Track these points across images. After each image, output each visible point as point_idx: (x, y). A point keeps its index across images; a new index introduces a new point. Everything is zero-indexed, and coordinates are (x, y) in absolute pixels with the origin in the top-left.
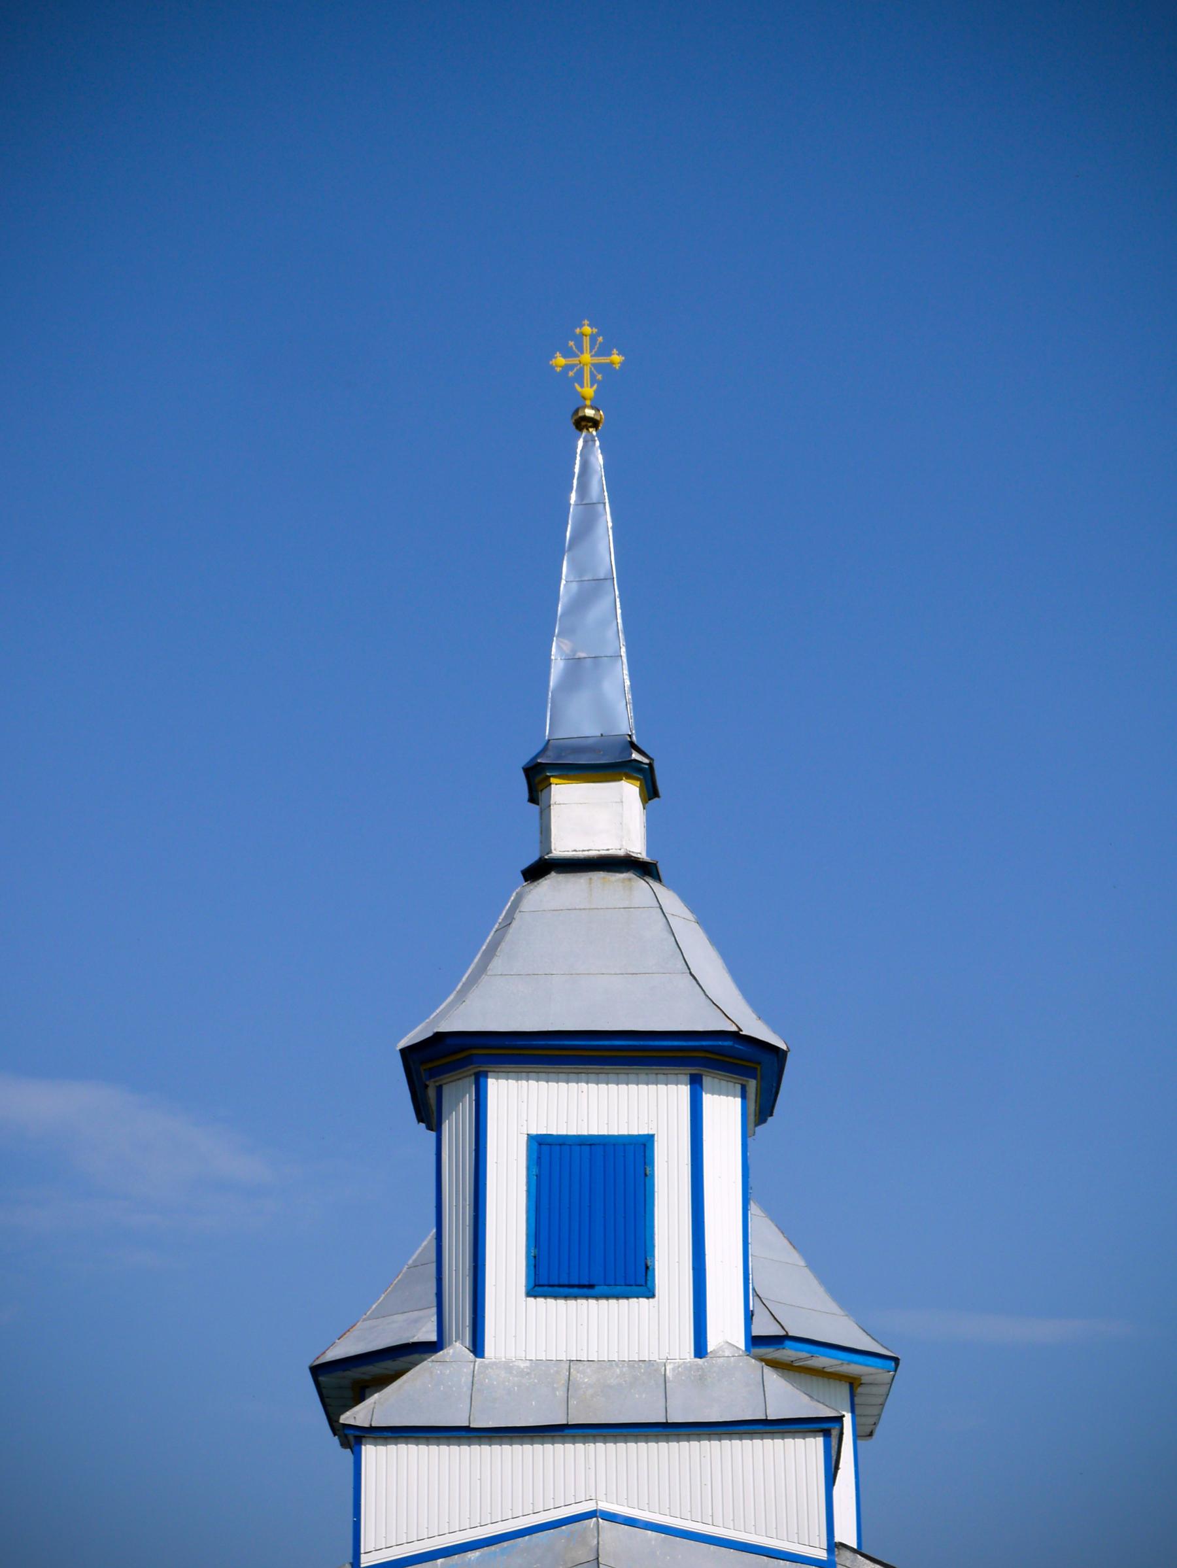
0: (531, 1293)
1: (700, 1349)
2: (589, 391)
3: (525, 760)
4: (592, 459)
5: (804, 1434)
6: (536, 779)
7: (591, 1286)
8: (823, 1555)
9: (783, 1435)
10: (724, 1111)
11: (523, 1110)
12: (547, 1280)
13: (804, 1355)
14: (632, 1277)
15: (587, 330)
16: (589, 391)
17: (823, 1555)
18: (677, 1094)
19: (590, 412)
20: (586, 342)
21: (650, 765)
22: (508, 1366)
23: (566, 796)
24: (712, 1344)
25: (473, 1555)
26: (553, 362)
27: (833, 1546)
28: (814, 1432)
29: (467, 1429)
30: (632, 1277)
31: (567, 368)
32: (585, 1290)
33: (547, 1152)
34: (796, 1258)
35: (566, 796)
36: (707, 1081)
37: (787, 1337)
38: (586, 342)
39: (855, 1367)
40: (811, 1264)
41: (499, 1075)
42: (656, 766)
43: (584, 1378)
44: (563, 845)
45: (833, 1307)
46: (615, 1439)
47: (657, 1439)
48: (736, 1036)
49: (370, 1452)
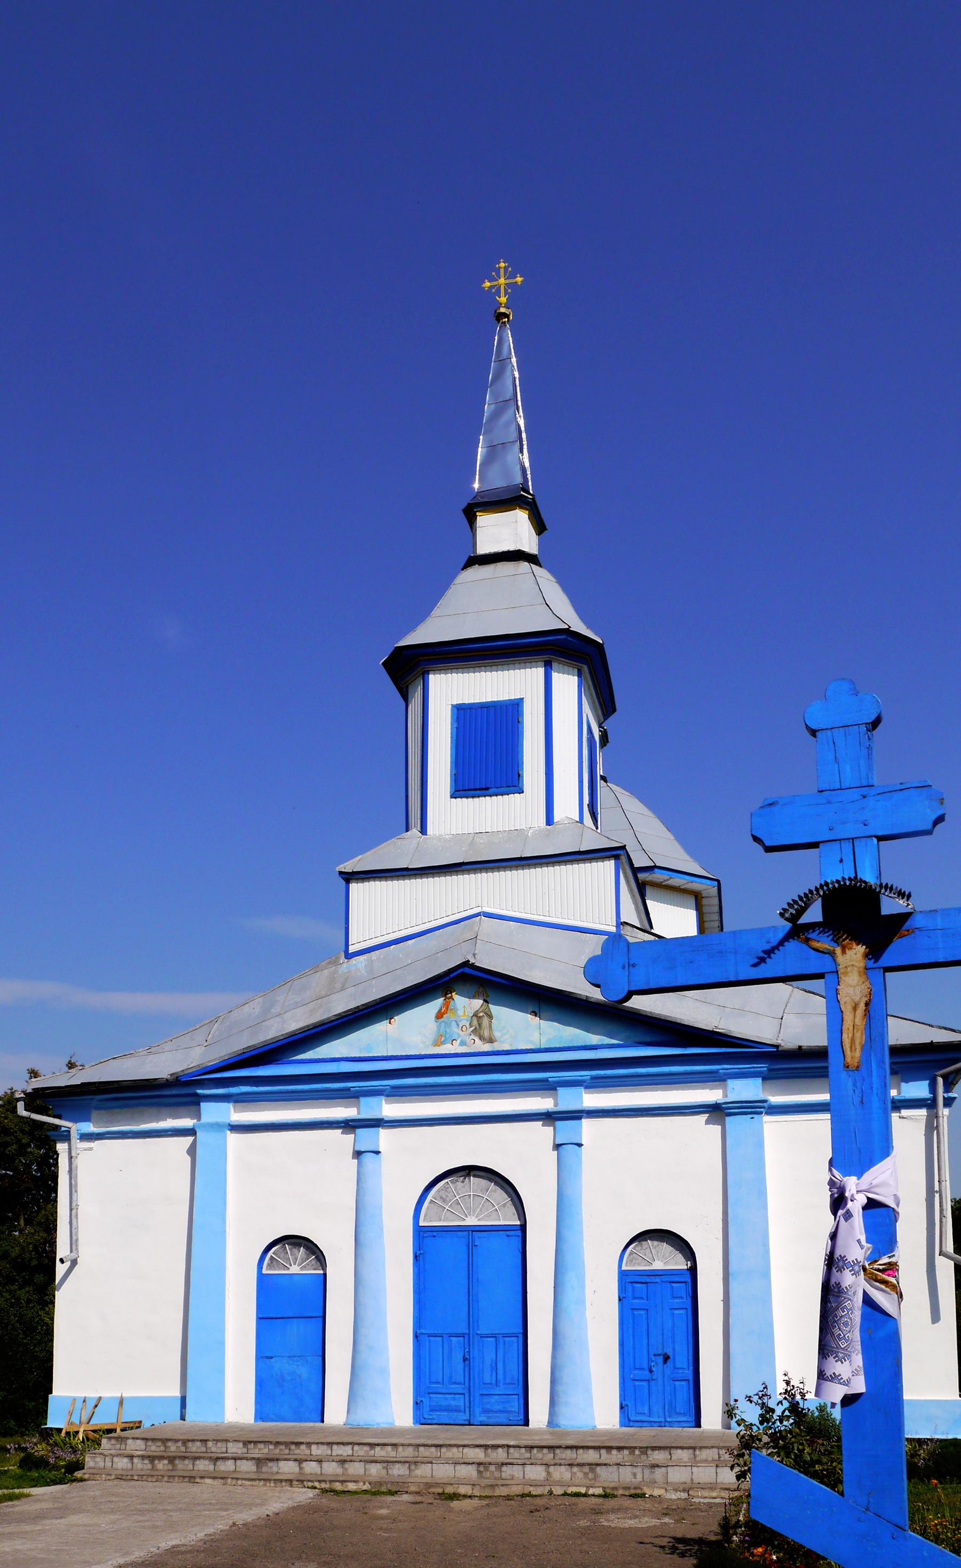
0: (453, 796)
1: (549, 820)
2: (503, 300)
3: (464, 505)
4: (505, 334)
5: (603, 859)
6: (470, 513)
7: (487, 789)
8: (614, 929)
9: (590, 860)
10: (567, 685)
11: (449, 690)
12: (466, 785)
13: (666, 877)
14: (507, 781)
15: (502, 265)
16: (503, 300)
17: (614, 929)
18: (536, 674)
19: (503, 310)
20: (502, 271)
21: (533, 499)
22: (439, 838)
23: (484, 520)
24: (557, 818)
25: (410, 942)
26: (484, 285)
27: (621, 924)
28: (609, 858)
29: (407, 869)
30: (507, 781)
31: (491, 287)
32: (484, 792)
33: (465, 715)
34: (669, 835)
35: (484, 520)
36: (555, 665)
37: (655, 867)
38: (502, 271)
39: (697, 885)
40: (678, 838)
41: (435, 671)
42: (536, 499)
43: (479, 840)
44: (483, 548)
45: (687, 857)
46: (492, 869)
47: (517, 868)
48: (567, 631)
49: (354, 887)
